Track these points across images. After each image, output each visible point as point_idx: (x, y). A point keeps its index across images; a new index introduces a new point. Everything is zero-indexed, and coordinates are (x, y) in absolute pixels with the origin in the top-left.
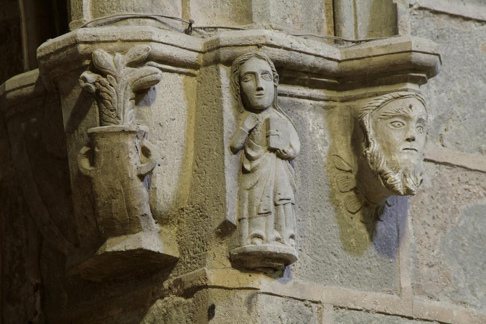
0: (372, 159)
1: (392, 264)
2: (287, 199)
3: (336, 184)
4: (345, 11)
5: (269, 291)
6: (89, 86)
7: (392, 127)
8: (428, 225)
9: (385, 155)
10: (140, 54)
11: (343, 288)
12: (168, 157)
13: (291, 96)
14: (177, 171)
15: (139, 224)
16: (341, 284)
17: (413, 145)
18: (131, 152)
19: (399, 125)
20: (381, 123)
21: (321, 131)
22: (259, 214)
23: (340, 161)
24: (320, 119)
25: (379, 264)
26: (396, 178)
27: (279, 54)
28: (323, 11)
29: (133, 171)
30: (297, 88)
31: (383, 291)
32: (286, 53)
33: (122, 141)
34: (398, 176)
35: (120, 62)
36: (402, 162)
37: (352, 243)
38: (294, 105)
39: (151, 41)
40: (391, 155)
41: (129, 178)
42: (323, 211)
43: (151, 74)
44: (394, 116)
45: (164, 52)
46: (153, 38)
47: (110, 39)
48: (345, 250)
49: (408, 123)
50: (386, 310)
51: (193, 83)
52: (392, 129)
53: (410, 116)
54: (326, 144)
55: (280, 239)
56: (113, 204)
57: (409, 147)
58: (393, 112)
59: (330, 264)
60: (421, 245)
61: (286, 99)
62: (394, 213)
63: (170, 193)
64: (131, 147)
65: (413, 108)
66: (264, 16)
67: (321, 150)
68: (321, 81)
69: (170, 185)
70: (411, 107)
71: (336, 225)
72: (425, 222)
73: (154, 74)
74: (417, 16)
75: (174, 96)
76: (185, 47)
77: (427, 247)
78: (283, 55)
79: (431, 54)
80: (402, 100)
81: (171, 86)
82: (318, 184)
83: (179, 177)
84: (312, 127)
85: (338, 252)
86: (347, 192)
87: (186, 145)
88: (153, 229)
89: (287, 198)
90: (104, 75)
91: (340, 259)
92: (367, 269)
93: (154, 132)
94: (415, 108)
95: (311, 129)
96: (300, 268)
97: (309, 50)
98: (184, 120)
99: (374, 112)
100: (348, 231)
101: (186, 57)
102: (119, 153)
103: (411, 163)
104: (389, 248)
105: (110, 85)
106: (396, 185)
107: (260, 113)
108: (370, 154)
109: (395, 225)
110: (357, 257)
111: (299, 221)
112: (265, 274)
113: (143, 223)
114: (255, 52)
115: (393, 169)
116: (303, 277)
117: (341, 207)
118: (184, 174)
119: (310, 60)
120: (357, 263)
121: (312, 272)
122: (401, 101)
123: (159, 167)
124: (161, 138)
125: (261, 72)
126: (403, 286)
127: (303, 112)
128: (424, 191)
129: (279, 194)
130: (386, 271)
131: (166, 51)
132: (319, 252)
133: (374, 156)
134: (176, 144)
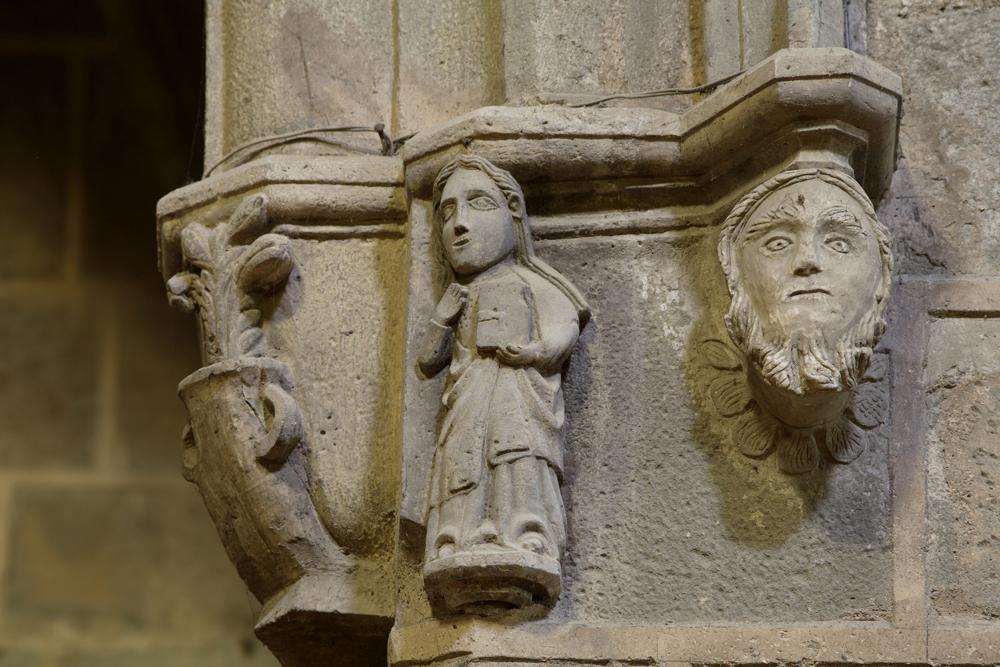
0: (737, 330)
1: (872, 554)
2: (517, 450)
3: (711, 400)
4: (713, 31)
5: (496, 654)
6: (178, 300)
7: (768, 253)
8: (992, 455)
9: (760, 316)
10: (248, 213)
11: (725, 623)
12: (340, 412)
13: (585, 233)
14: (363, 437)
15: (292, 560)
16: (719, 613)
17: (816, 281)
18: (235, 416)
19: (779, 244)
20: (750, 248)
21: (674, 295)
22: (454, 492)
23: (722, 349)
24: (670, 270)
25: (830, 558)
26: (776, 361)
27: (509, 149)
28: (684, 44)
29: (246, 454)
30: (603, 215)
31: (841, 617)
32: (535, 144)
33: (216, 397)
34: (782, 355)
35: (217, 239)
36: (788, 323)
37: (754, 523)
38: (597, 251)
39: (265, 183)
40: (768, 312)
41: (240, 469)
42: (673, 465)
43: (262, 249)
44: (769, 229)
45: (302, 199)
46: (269, 176)
47: (203, 199)
48: (733, 539)
49: (798, 237)
50: (847, 656)
51: (399, 250)
52: (768, 256)
53: (798, 221)
54: (685, 319)
55: (494, 537)
56: (237, 528)
57: (803, 288)
58: (766, 220)
59: (689, 576)
60: (968, 503)
61: (574, 242)
62: (882, 443)
63: (354, 486)
64: (235, 406)
65: (806, 201)
66: (526, 82)
67: (671, 334)
68: (654, 189)
69: (350, 469)
70: (801, 200)
71: (709, 489)
72: (981, 450)
73: (267, 247)
74: (967, 10)
75: (349, 285)
76: (354, 179)
77: (984, 503)
78: (532, 151)
79: (826, 77)
80: (785, 190)
81: (341, 267)
82: (660, 408)
83: (370, 451)
84: (648, 290)
85: (713, 547)
86: (738, 414)
87: (382, 380)
88: (330, 568)
89: (515, 448)
90: (197, 270)
91: (718, 561)
92: (798, 572)
93: (304, 365)
94: (813, 201)
95: (645, 295)
96: (601, 594)
97: (591, 129)
98: (378, 330)
99: (738, 228)
100: (745, 497)
101: (361, 201)
102: (217, 423)
103: (809, 321)
104: (865, 526)
105: (207, 289)
106: (777, 376)
107: (472, 280)
108: (731, 320)
109: (884, 467)
110: (768, 552)
111: (603, 493)
112: (483, 617)
113: (301, 559)
114: (459, 157)
115: (775, 342)
116: (606, 612)
117: (726, 450)
118: (380, 441)
119: (602, 149)
120: (767, 564)
121: (635, 599)
122: (781, 193)
123: (324, 436)
124: (322, 376)
125: (466, 195)
126: (898, 599)
127: (622, 262)
128: (978, 383)
129: (496, 442)
130: (852, 572)
131: (308, 196)
132: (657, 553)
133: (738, 323)
134: (357, 382)
